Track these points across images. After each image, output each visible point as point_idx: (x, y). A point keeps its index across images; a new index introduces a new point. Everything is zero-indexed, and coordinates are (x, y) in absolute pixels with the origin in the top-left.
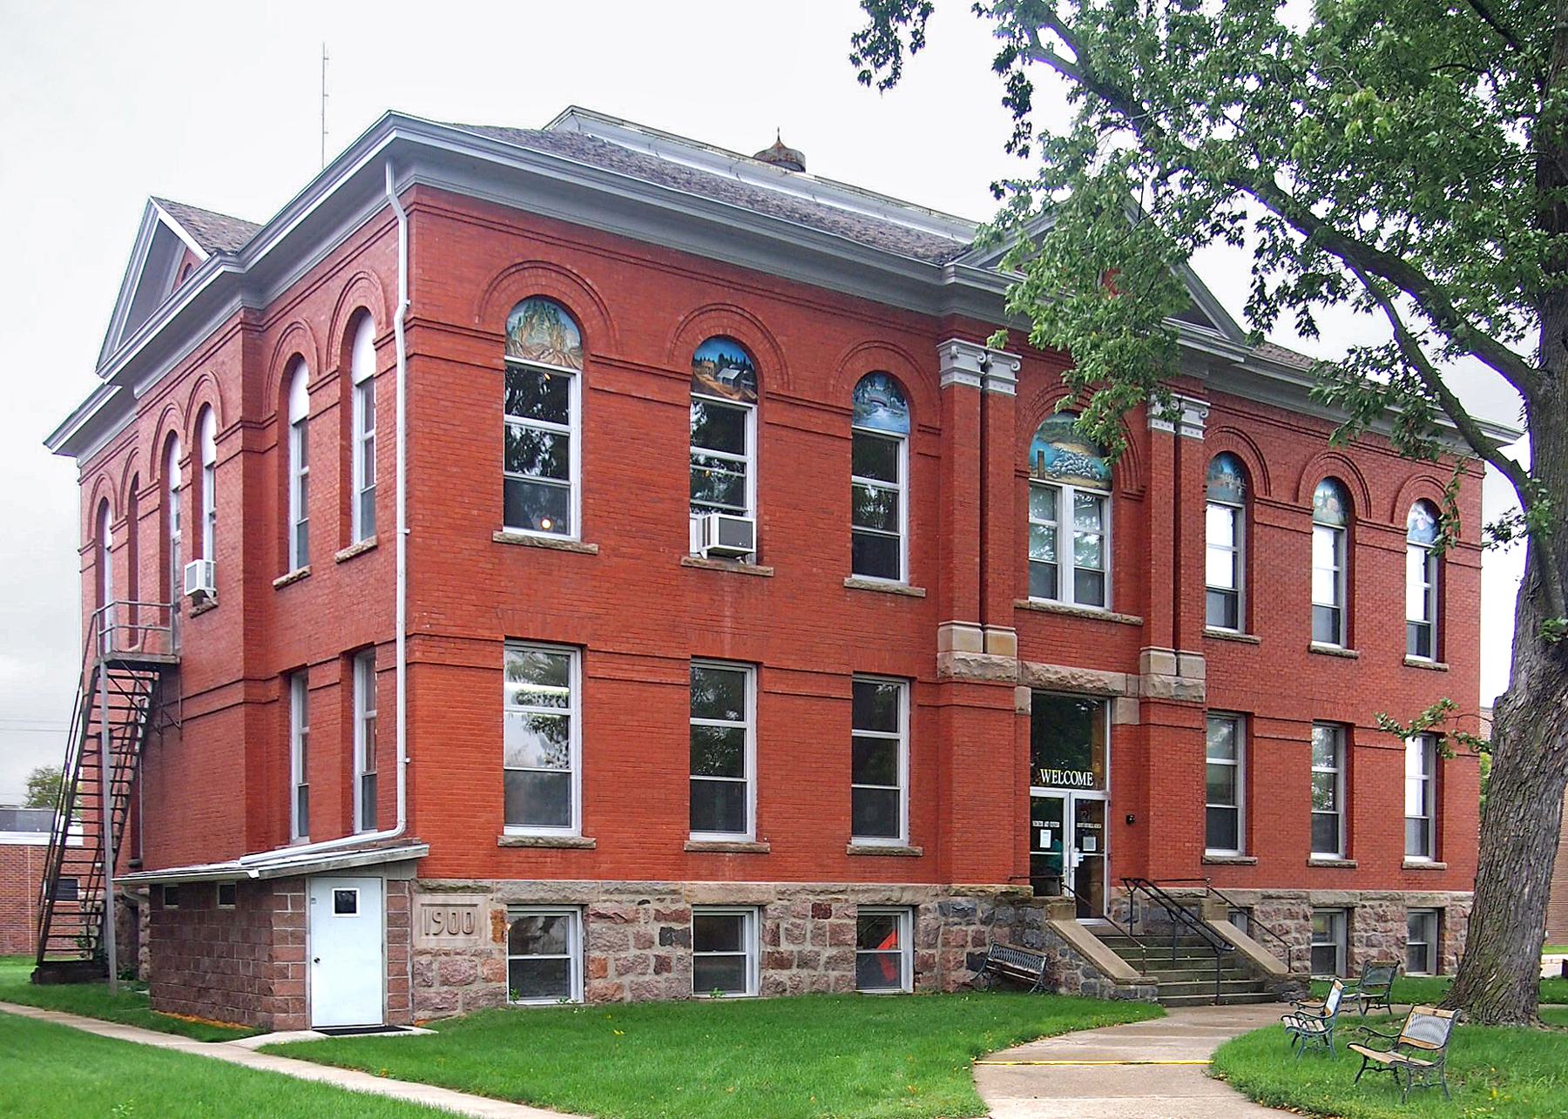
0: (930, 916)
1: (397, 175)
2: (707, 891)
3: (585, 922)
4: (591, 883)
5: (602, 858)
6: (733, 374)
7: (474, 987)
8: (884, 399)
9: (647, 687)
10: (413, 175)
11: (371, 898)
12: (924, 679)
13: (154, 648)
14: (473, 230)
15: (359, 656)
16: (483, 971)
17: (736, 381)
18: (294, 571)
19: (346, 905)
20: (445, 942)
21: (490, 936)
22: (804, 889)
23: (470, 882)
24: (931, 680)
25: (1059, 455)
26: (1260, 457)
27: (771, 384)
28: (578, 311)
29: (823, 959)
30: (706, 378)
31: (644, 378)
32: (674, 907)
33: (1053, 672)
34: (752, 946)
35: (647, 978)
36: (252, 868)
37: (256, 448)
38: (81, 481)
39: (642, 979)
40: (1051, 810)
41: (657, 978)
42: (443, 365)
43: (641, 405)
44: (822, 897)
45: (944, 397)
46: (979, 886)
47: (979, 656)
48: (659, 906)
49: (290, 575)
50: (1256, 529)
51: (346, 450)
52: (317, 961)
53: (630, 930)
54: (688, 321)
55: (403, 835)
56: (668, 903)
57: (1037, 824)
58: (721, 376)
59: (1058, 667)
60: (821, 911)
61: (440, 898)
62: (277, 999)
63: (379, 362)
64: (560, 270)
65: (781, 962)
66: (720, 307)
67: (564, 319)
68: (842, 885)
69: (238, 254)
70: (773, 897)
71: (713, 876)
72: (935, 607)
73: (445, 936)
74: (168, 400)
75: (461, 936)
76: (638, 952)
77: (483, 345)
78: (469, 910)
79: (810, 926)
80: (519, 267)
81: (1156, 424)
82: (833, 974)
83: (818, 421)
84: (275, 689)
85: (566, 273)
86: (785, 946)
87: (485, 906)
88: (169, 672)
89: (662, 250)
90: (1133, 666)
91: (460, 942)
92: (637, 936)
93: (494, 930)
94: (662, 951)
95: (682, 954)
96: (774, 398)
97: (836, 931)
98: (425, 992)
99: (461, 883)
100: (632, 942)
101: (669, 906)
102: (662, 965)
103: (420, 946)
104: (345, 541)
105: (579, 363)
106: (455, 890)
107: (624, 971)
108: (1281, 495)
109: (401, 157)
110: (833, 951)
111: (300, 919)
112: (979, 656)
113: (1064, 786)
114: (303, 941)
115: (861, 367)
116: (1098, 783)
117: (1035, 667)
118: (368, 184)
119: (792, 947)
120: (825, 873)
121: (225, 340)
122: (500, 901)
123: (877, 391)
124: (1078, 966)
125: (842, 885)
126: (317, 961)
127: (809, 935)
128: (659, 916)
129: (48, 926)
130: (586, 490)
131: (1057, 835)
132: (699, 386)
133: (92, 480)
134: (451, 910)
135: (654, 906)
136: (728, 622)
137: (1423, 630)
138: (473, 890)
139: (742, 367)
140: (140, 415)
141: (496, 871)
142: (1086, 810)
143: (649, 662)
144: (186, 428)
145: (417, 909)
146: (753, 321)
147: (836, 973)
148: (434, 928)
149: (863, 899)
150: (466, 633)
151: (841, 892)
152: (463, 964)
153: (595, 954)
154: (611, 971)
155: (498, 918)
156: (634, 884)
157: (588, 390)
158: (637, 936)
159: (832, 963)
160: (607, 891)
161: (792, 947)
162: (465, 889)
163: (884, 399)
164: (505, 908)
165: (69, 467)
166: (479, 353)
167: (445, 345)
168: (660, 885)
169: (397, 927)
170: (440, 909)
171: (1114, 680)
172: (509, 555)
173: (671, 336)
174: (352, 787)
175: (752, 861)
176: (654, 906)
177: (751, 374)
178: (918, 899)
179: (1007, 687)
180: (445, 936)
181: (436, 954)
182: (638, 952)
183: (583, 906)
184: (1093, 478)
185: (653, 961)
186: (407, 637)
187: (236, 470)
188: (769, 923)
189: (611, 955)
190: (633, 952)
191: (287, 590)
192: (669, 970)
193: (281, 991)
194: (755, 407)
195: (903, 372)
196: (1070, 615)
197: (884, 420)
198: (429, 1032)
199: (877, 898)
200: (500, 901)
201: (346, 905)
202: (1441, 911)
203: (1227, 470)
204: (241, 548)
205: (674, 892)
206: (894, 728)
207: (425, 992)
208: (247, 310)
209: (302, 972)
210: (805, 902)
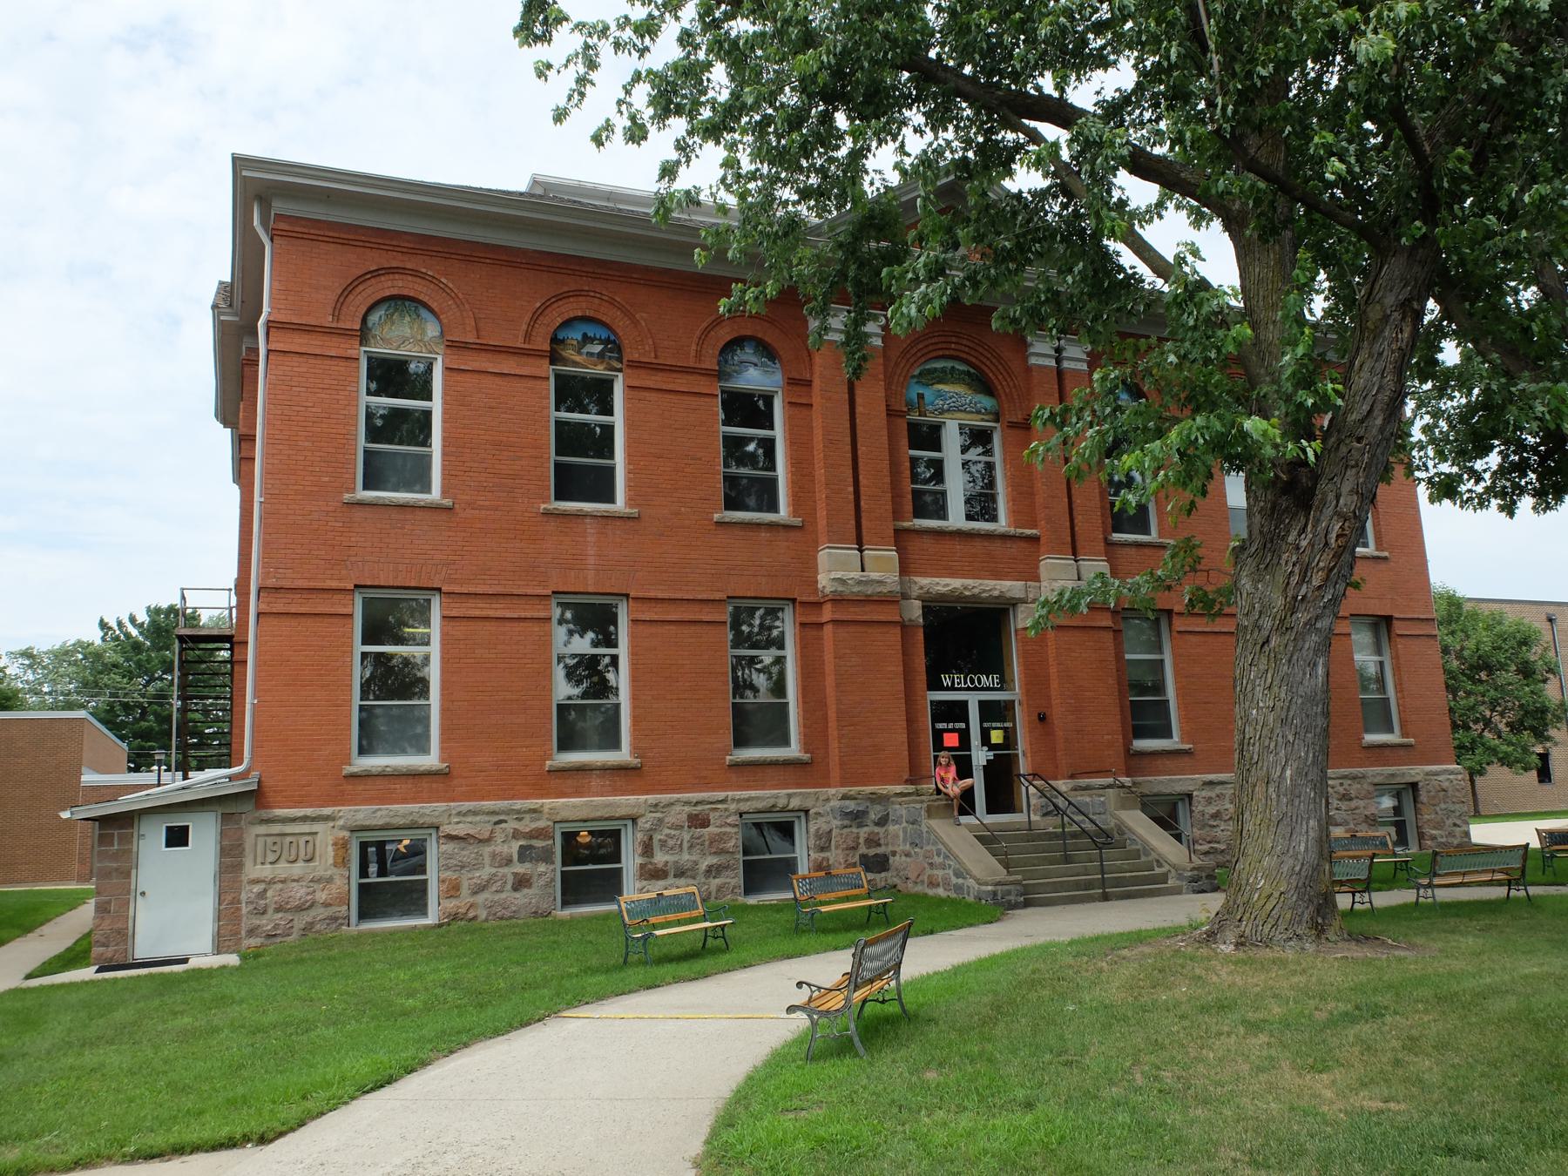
0: (821, 820)
4: (441, 806)
5: (455, 782)
6: (597, 348)
7: (312, 913)
8: (755, 360)
9: (507, 626)
11: (205, 833)
12: (804, 599)
16: (322, 896)
17: (601, 355)
19: (177, 837)
21: (331, 861)
22: (678, 801)
23: (309, 811)
24: (812, 599)
25: (940, 395)
27: (631, 354)
29: (703, 866)
32: (534, 825)
35: (503, 896)
39: (496, 897)
40: (957, 711)
41: (517, 895)
42: (296, 358)
43: (498, 380)
44: (699, 808)
47: (857, 574)
48: (516, 825)
52: (143, 894)
53: (487, 850)
57: (940, 726)
58: (584, 350)
59: (948, 580)
60: (698, 821)
61: (276, 828)
64: (415, 273)
65: (657, 874)
66: (578, 293)
67: (424, 313)
68: (721, 795)
76: (494, 870)
77: (336, 339)
79: (686, 837)
85: (423, 276)
86: (660, 858)
87: (326, 837)
89: (524, 252)
92: (494, 855)
93: (336, 856)
94: (520, 869)
95: (550, 872)
99: (309, 811)
100: (487, 860)
101: (527, 825)
105: (440, 349)
106: (294, 820)
107: (479, 889)
110: (713, 860)
112: (857, 574)
113: (968, 689)
114: (128, 875)
119: (667, 858)
120: (706, 784)
122: (342, 828)
123: (748, 353)
125: (721, 795)
127: (686, 845)
128: (516, 835)
131: (965, 736)
134: (289, 839)
136: (591, 560)
138: (314, 819)
139: (606, 342)
141: (338, 799)
147: (718, 881)
150: (312, 584)
154: (465, 891)
155: (342, 846)
158: (494, 855)
159: (712, 871)
160: (459, 814)
161: (667, 858)
162: (304, 819)
163: (755, 360)
164: (346, 834)
167: (298, 342)
168: (519, 804)
170: (277, 839)
172: (359, 514)
176: (511, 825)
177: (614, 347)
178: (808, 804)
180: (282, 865)
181: (272, 882)
182: (494, 870)
184: (978, 412)
188: (639, 836)
190: (486, 872)
194: (620, 375)
196: (959, 534)
197: (754, 377)
199: (760, 805)
200: (342, 828)
201: (177, 837)
202: (1414, 786)
205: (534, 811)
210: (679, 814)
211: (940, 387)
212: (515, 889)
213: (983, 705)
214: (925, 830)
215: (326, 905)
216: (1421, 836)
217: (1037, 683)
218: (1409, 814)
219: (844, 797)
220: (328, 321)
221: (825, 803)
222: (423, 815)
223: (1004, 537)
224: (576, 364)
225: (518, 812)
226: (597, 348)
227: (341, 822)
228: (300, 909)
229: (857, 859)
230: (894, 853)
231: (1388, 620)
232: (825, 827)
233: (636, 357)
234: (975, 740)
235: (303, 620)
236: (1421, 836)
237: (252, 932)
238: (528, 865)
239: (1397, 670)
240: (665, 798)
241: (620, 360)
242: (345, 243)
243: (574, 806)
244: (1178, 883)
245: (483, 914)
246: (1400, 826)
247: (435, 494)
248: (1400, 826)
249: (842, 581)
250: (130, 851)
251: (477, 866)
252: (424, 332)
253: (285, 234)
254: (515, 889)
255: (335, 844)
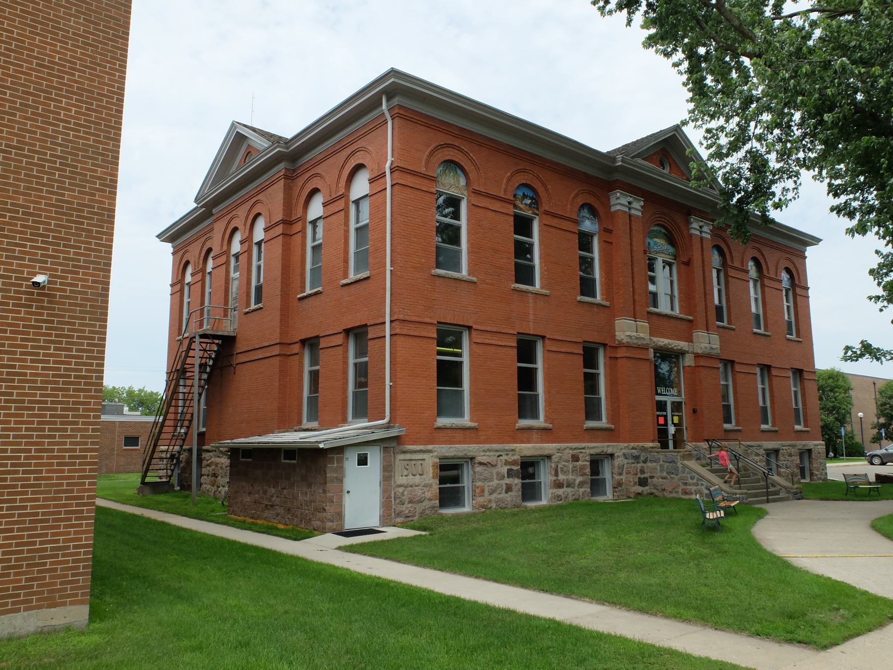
1: (388, 101)
2: (528, 449)
3: (473, 467)
6: (529, 202)
7: (424, 504)
8: (588, 216)
10: (396, 101)
11: (375, 457)
13: (228, 328)
14: (422, 128)
15: (358, 334)
18: (308, 291)
19: (363, 461)
20: (411, 480)
25: (656, 243)
26: (729, 247)
27: (545, 207)
28: (466, 168)
29: (577, 482)
30: (518, 203)
31: (494, 201)
33: (663, 342)
34: (545, 477)
35: (502, 496)
36: (320, 442)
37: (288, 233)
38: (173, 254)
40: (661, 406)
41: (507, 495)
42: (409, 190)
45: (612, 216)
46: (641, 444)
49: (305, 294)
50: (730, 279)
51: (347, 232)
52: (348, 492)
53: (494, 471)
54: (512, 176)
55: (389, 422)
56: (510, 456)
59: (662, 340)
60: (575, 458)
61: (408, 456)
62: (328, 515)
63: (371, 188)
64: (459, 149)
65: (558, 485)
67: (459, 172)
69: (286, 143)
70: (554, 452)
71: (529, 442)
72: (609, 311)
73: (411, 477)
74: (234, 213)
75: (418, 476)
77: (426, 181)
78: (420, 462)
79: (571, 466)
80: (442, 146)
81: (693, 231)
82: (582, 490)
83: (565, 225)
84: (296, 348)
86: (561, 477)
88: (228, 342)
89: (501, 144)
90: (690, 340)
91: (417, 479)
92: (498, 474)
95: (517, 482)
96: (547, 213)
97: (582, 468)
98: (401, 508)
102: (509, 489)
103: (399, 482)
104: (346, 276)
105: (466, 193)
107: (492, 492)
108: (737, 264)
109: (391, 92)
111: (341, 470)
112: (634, 334)
115: (580, 201)
116: (679, 395)
117: (655, 339)
118: (374, 103)
120: (576, 439)
121: (272, 184)
122: (436, 457)
123: (585, 213)
124: (702, 485)
126: (348, 492)
128: (507, 463)
129: (149, 464)
130: (470, 252)
132: (515, 206)
133: (181, 253)
134: (413, 462)
135: (504, 458)
136: (531, 317)
137: (789, 323)
139: (532, 198)
140: (215, 221)
142: (677, 407)
143: (499, 335)
144: (245, 225)
145: (397, 462)
146: (538, 177)
148: (405, 473)
149: (593, 452)
151: (584, 448)
152: (418, 492)
153: (479, 484)
154: (486, 493)
156: (495, 446)
157: (472, 206)
158: (498, 474)
159: (581, 484)
160: (484, 451)
165: (168, 247)
166: (424, 185)
167: (409, 180)
169: (388, 471)
171: (682, 345)
172: (438, 281)
173: (505, 180)
174: (347, 397)
175: (546, 433)
176: (504, 458)
177: (536, 203)
178: (614, 451)
179: (645, 348)
181: (406, 487)
183: (472, 459)
185: (504, 486)
186: (391, 322)
187: (278, 244)
189: (487, 484)
191: (306, 301)
192: (511, 491)
193: (330, 509)
195: (596, 205)
197: (588, 225)
198: (418, 533)
199: (598, 451)
201: (363, 461)
203: (716, 253)
204: (279, 280)
205: (513, 450)
206: (356, 365)
207: (403, 508)
208: (286, 169)
209: (341, 498)
210: (568, 454)
211: (656, 240)
212: (506, 492)
213: (673, 403)
214: (680, 466)
215: (430, 500)
216: (812, 474)
217: (693, 391)
218: (807, 464)
219: (633, 448)
220: (423, 170)
221: (618, 448)
222: (469, 451)
223: (599, 305)
224: (521, 209)
225: (507, 450)
226: (529, 202)
227: (435, 454)
228: (420, 501)
229: (637, 480)
230: (652, 477)
231: (732, 362)
232: (622, 463)
233: (547, 208)
234: (670, 422)
235: (414, 339)
236: (812, 474)
237: (398, 515)
238: (511, 479)
239: (803, 395)
240: (563, 445)
241: (538, 209)
242: (428, 126)
243: (529, 448)
244: (786, 495)
245: (494, 505)
246: (802, 470)
247: (464, 272)
248: (802, 470)
249: (630, 336)
250: (342, 467)
251: (491, 480)
252: (459, 183)
253: (400, 116)
254: (506, 492)
255: (433, 466)
